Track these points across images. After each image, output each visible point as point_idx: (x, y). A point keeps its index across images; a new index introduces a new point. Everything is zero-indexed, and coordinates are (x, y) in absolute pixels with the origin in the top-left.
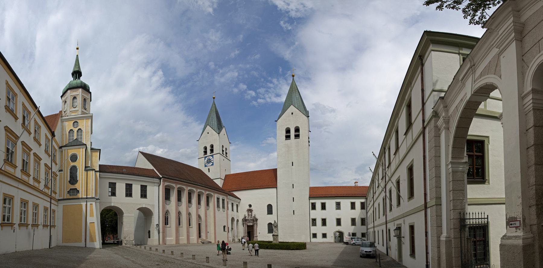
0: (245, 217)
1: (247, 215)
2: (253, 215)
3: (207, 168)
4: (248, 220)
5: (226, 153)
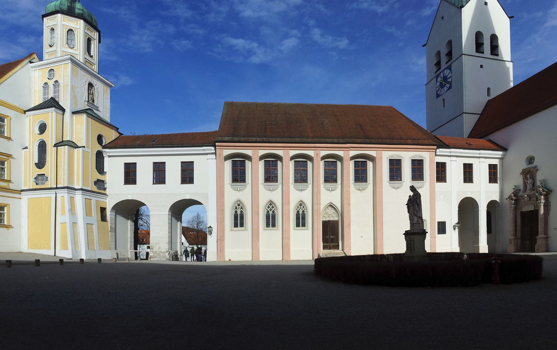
1: (522, 188)
3: (441, 98)
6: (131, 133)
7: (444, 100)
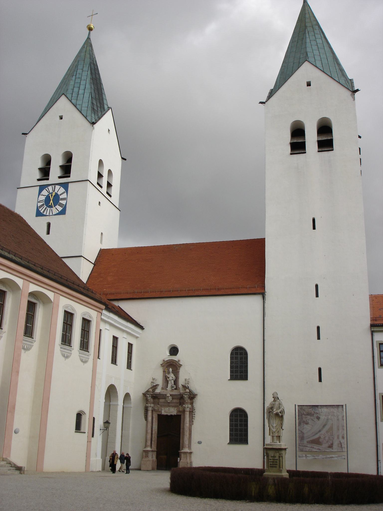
0: (155, 387)
1: (160, 381)
2: (181, 382)
4: (164, 397)
7: (49, 225)
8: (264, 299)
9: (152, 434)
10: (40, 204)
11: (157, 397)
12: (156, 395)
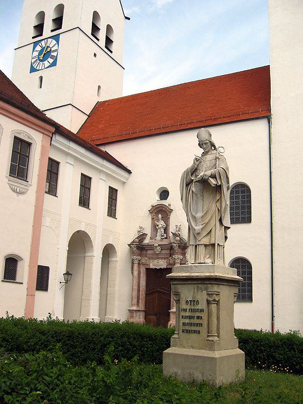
0: (142, 237)
1: (148, 230)
2: (172, 229)
3: (36, 75)
4: (151, 247)
5: (109, 41)
6: (220, 355)
7: (41, 78)
8: (269, 123)
9: (139, 291)
10: (33, 61)
11: (144, 248)
12: (143, 245)
